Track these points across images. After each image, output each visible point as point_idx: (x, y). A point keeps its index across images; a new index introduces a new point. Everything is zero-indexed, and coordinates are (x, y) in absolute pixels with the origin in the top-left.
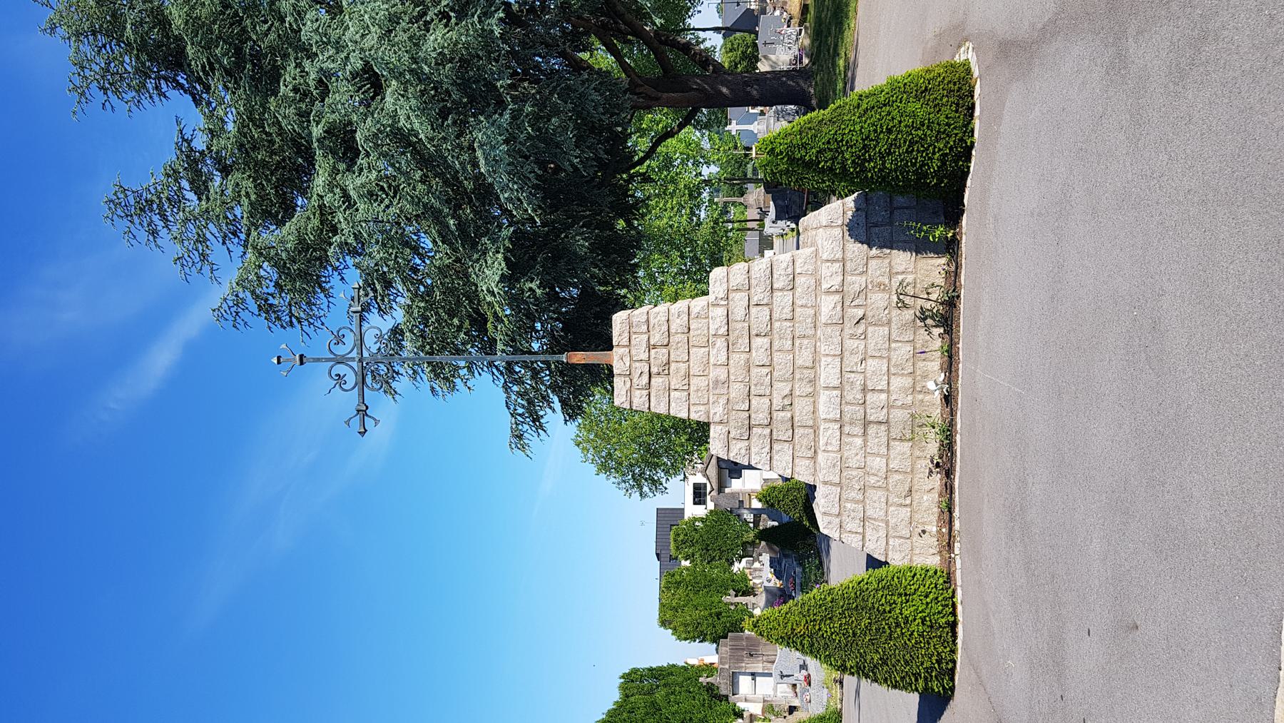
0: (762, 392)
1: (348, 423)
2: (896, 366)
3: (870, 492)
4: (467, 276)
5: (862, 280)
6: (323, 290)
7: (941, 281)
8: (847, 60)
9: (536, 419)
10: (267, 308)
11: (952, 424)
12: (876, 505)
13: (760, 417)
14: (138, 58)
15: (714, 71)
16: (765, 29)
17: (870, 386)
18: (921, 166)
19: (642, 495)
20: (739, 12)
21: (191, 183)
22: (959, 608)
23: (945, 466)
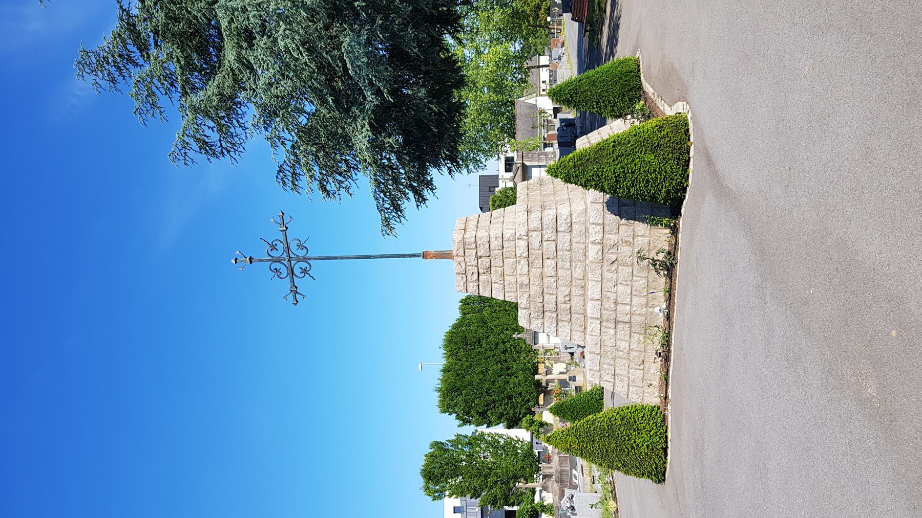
3: (618, 360)
9: (397, 208)
10: (205, 146)
13: (550, 306)
17: (619, 300)
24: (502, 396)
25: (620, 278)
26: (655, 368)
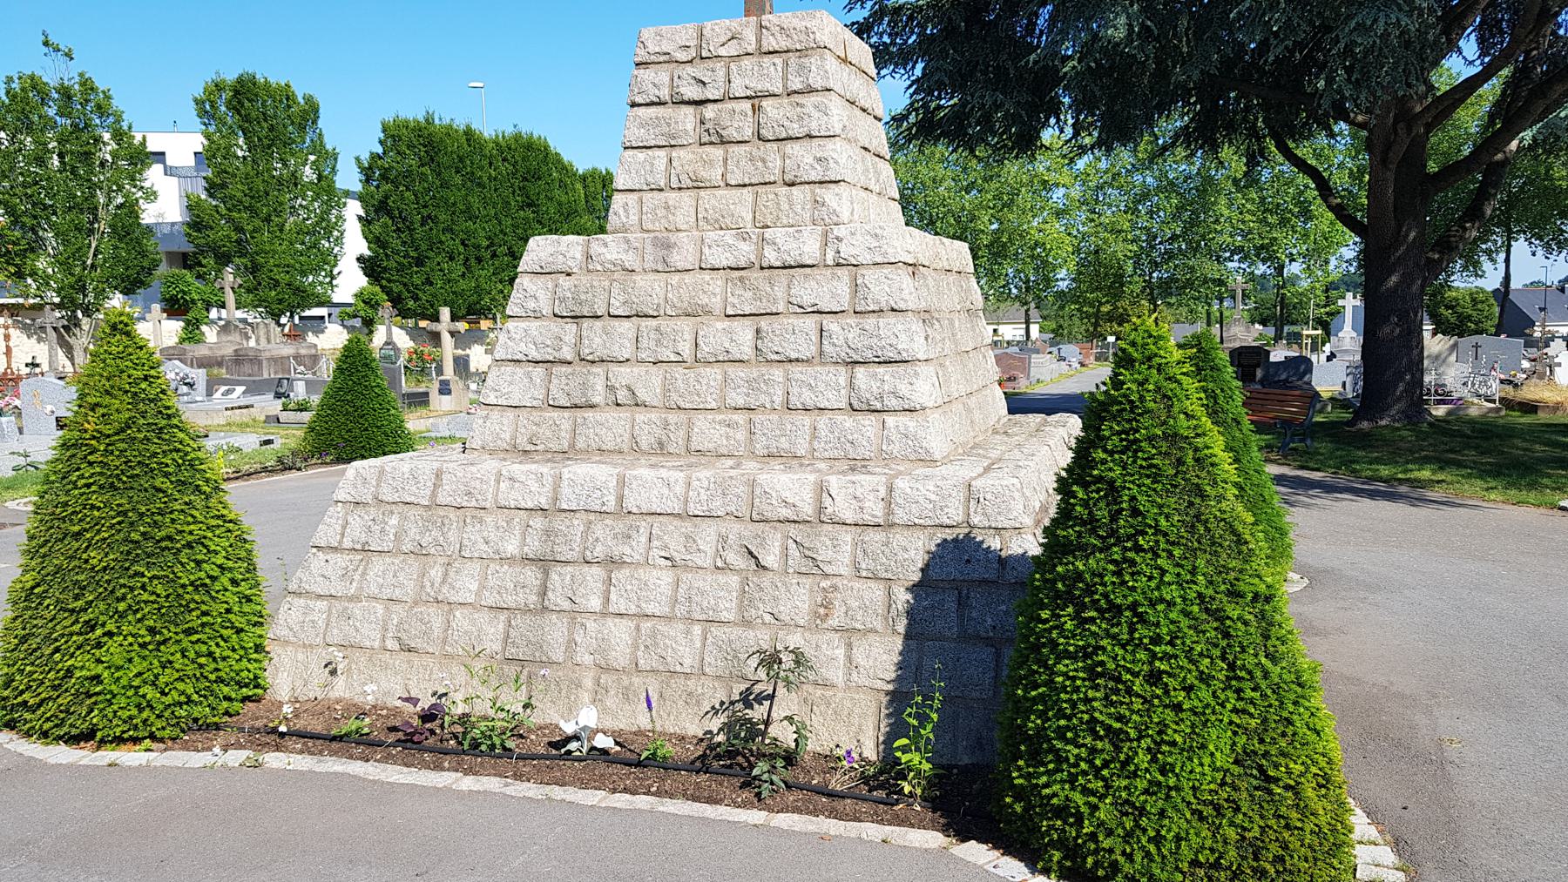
0: (644, 343)
2: (654, 634)
3: (414, 564)
8: (1430, 483)
13: (596, 338)
15: (1430, 261)
16: (1498, 347)
18: (1056, 752)
23: (424, 736)
24: (424, 247)
26: (385, 687)
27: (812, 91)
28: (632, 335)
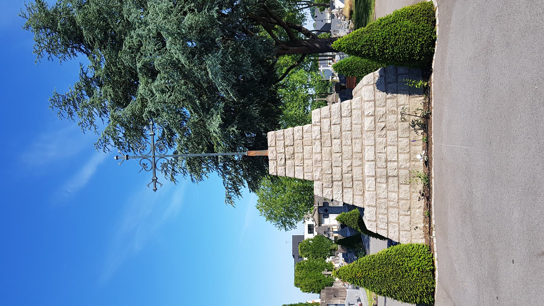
1: (148, 185)
2: (401, 149)
3: (390, 209)
4: (205, 127)
5: (383, 110)
6: (143, 136)
7: (422, 108)
9: (237, 190)
11: (429, 175)
12: (394, 215)
13: (337, 177)
14: (63, 37)
19: (286, 230)
20: (323, 24)
21: (87, 92)
22: (436, 263)
23: (427, 195)
25: (389, 140)
27: (284, 134)
28: (336, 168)
